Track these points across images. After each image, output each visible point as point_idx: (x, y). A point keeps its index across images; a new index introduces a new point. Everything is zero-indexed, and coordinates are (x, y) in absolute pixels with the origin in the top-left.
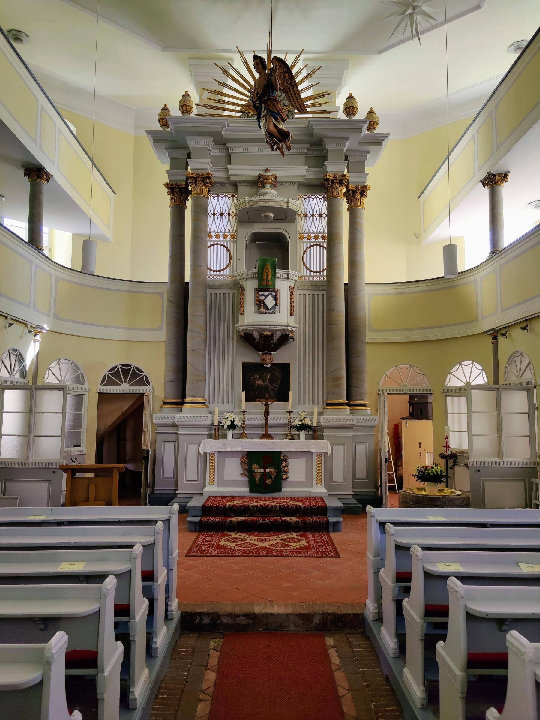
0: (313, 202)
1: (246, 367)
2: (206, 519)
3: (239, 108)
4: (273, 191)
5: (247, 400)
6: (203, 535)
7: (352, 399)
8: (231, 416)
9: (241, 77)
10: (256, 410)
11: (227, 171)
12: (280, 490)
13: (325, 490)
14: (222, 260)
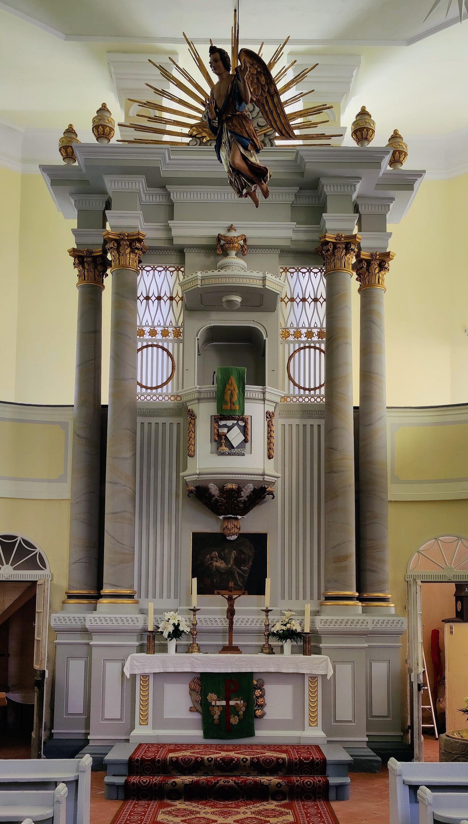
0: (304, 279)
1: (199, 539)
2: (134, 779)
3: (186, 130)
4: (241, 262)
5: (199, 592)
6: (130, 805)
7: (366, 589)
8: (175, 618)
9: (191, 80)
10: (212, 609)
11: (169, 229)
12: (251, 734)
13: (322, 734)
14: (158, 372)
